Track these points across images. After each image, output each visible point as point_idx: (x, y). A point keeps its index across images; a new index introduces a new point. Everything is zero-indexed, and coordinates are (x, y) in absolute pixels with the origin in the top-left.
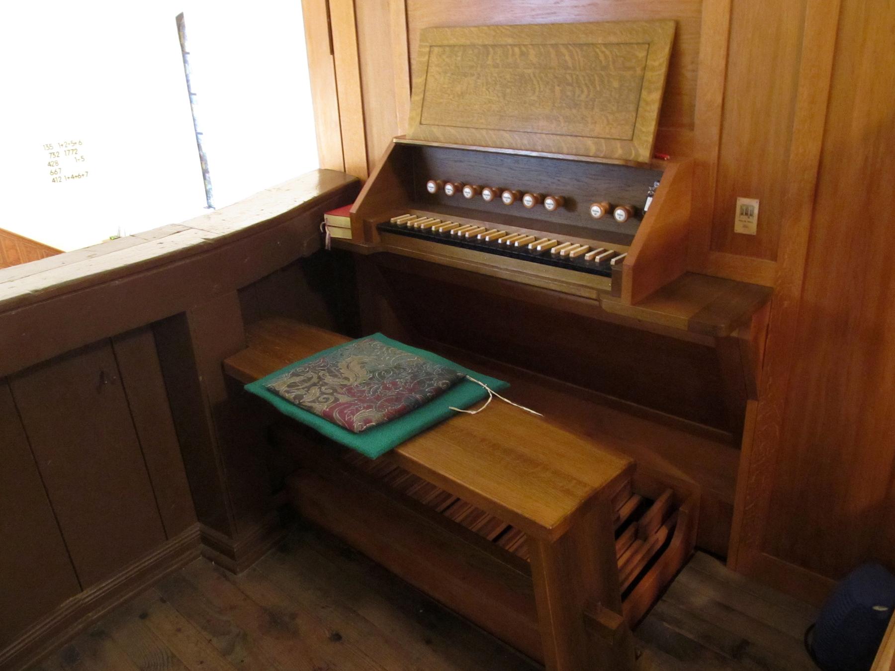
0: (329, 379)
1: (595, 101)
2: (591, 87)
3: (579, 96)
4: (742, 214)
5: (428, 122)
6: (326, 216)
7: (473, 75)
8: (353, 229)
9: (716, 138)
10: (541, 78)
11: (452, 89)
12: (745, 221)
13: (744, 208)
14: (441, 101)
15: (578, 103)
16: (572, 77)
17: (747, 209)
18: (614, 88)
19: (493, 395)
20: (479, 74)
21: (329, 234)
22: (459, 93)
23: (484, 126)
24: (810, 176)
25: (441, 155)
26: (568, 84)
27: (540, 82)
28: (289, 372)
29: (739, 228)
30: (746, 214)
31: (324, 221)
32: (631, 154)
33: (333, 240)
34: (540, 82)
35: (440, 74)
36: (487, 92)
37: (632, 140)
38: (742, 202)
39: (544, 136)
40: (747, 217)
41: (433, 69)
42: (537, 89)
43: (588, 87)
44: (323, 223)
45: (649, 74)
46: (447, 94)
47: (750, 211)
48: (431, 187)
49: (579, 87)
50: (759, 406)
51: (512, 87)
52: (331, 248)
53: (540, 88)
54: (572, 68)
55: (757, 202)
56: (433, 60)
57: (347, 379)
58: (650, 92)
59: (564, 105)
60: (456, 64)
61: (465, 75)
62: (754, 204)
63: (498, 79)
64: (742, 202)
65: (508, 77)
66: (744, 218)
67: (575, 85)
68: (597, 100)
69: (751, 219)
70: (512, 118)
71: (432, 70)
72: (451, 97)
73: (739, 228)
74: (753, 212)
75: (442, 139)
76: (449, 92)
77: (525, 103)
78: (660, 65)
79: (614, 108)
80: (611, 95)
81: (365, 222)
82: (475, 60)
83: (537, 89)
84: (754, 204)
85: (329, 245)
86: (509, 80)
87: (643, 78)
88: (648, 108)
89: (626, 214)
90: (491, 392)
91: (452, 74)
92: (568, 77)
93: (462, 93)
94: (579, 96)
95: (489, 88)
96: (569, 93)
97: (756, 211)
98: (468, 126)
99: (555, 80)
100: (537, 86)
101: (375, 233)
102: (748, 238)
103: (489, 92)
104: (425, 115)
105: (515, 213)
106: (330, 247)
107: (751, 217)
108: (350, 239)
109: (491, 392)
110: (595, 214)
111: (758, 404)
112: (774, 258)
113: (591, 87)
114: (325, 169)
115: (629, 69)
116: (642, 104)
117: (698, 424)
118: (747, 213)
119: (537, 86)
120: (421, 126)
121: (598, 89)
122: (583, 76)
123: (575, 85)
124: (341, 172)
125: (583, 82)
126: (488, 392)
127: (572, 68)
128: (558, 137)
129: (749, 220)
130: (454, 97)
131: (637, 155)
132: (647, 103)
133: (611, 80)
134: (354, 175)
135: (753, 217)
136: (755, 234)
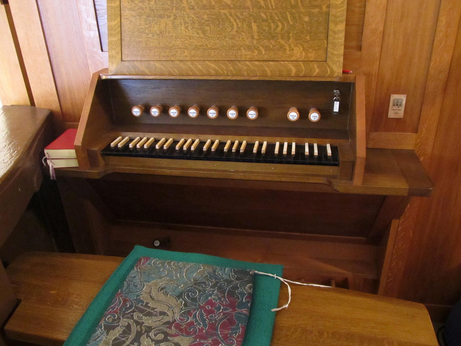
0: (148, 321)
1: (290, 33)
2: (284, 22)
3: (275, 30)
4: (394, 105)
5: (129, 59)
6: (46, 151)
7: (169, 17)
8: (78, 158)
9: (378, 55)
10: (238, 17)
11: (149, 29)
12: (396, 110)
13: (396, 101)
14: (141, 39)
15: (275, 35)
16: (265, 14)
17: (398, 102)
18: (306, 22)
19: (290, 284)
20: (175, 15)
21: (52, 166)
22: (158, 32)
23: (188, 59)
24: (443, 76)
25: (123, 83)
26: (264, 21)
27: (237, 20)
28: (101, 327)
29: (391, 114)
30: (397, 105)
31: (45, 156)
32: (327, 72)
33: (57, 170)
34: (237, 20)
35: (134, 16)
36: (187, 30)
37: (326, 61)
38: (394, 97)
39: (247, 63)
40: (397, 107)
41: (126, 13)
42: (235, 26)
43: (282, 23)
44: (45, 157)
45: (333, 11)
46: (145, 33)
47: (400, 103)
48: (136, 112)
49: (274, 22)
50: (400, 222)
51: (211, 25)
52: (56, 177)
53: (237, 24)
54: (265, 8)
55: (405, 96)
56: (124, 5)
57: (163, 313)
58: (336, 24)
59: (262, 37)
60: (150, 8)
61: (161, 16)
62: (403, 98)
63: (195, 19)
64: (394, 97)
65: (205, 17)
66: (396, 107)
67: (270, 21)
68: (291, 32)
69: (400, 108)
70: (214, 50)
71: (125, 14)
72: (150, 35)
73: (391, 114)
74: (402, 104)
75: (147, 71)
76: (147, 31)
77: (225, 38)
78: (342, 3)
79: (308, 38)
80: (303, 28)
81: (88, 150)
82: (169, 4)
83: (235, 26)
84: (403, 98)
85: (54, 175)
86: (207, 19)
87: (328, 14)
88: (337, 36)
89: (319, 115)
90: (284, 280)
91: (148, 16)
92: (263, 15)
93: (161, 32)
94: (275, 30)
95: (187, 26)
96: (266, 29)
97: (404, 102)
98: (172, 59)
99: (251, 18)
100: (235, 23)
101: (100, 158)
102: (398, 120)
103: (189, 30)
104: (125, 51)
105: (223, 123)
106: (55, 177)
107: (400, 107)
108: (77, 167)
109: (284, 280)
110: (293, 118)
111: (399, 221)
112: (416, 131)
113: (284, 22)
114: (12, 106)
115: (316, 7)
116: (330, 33)
117: (347, 237)
118: (397, 104)
119: (235, 23)
120: (123, 62)
121: (291, 23)
122: (276, 14)
123: (270, 21)
124: (27, 106)
125: (277, 18)
126: (282, 281)
127: (265, 8)
128: (261, 63)
129: (399, 109)
130: (153, 36)
131: (332, 71)
132: (335, 33)
133: (302, 15)
134: (44, 107)
135: (402, 106)
136: (402, 117)
